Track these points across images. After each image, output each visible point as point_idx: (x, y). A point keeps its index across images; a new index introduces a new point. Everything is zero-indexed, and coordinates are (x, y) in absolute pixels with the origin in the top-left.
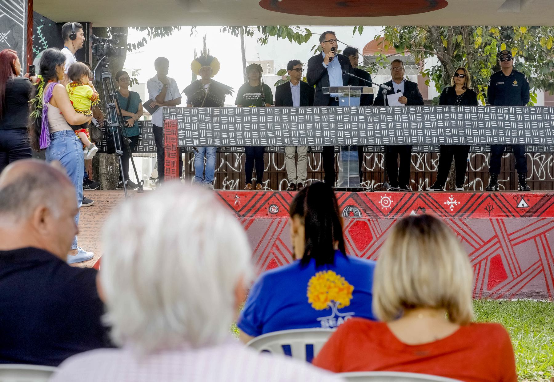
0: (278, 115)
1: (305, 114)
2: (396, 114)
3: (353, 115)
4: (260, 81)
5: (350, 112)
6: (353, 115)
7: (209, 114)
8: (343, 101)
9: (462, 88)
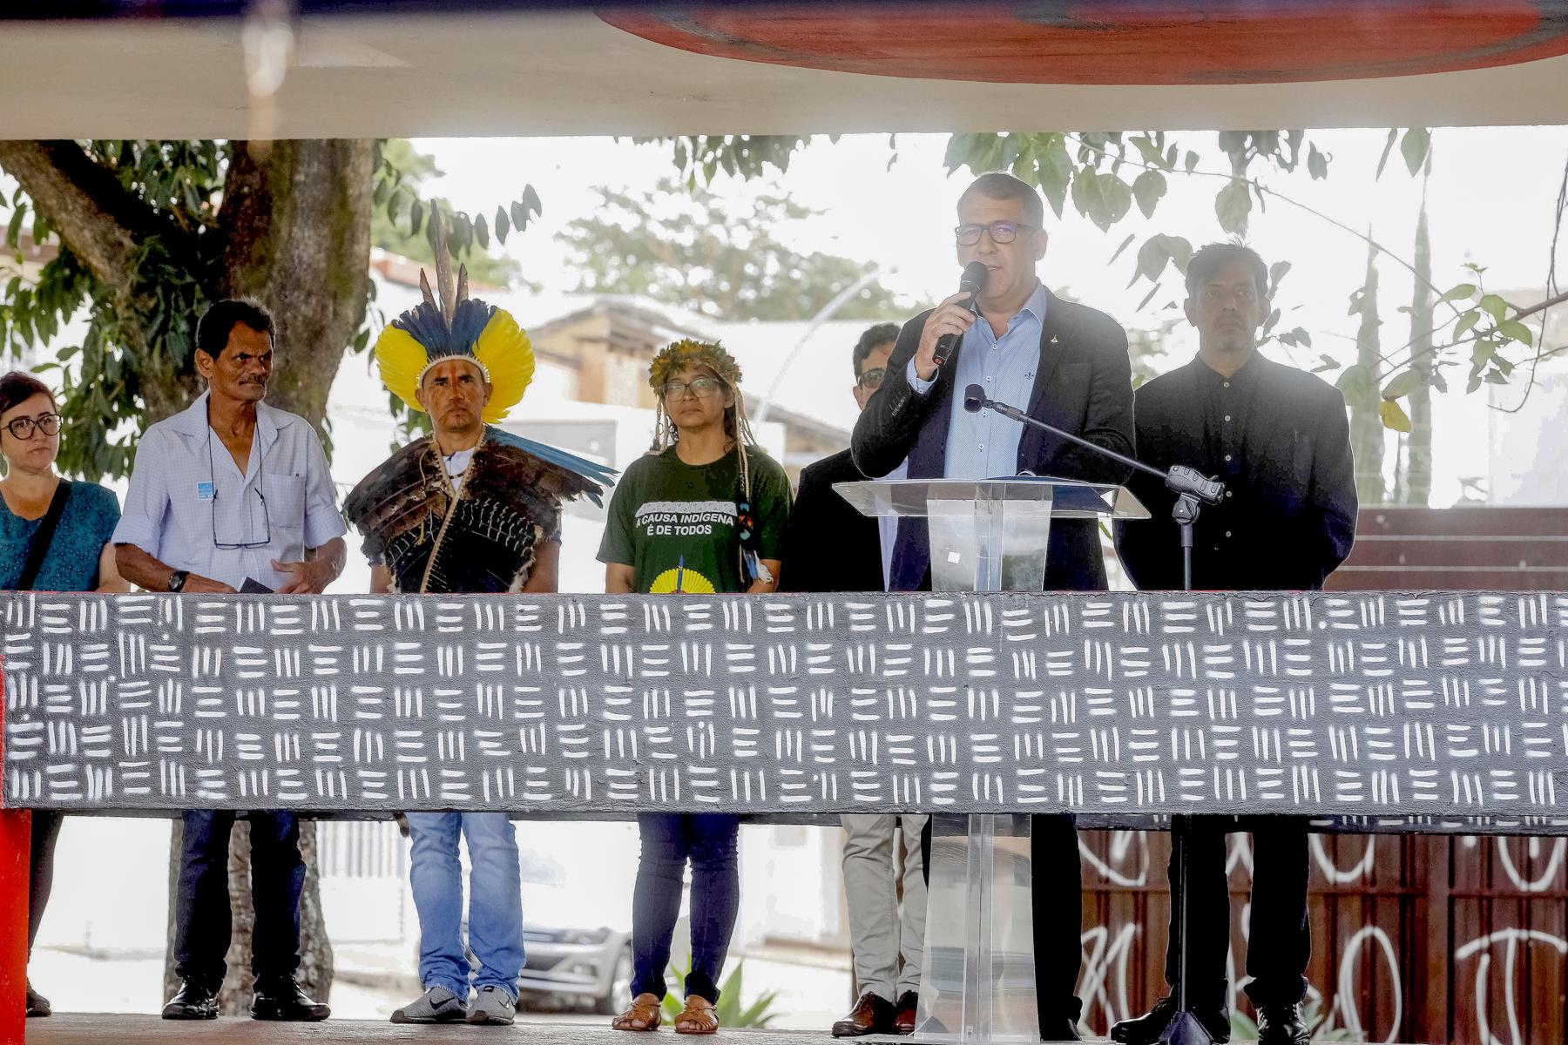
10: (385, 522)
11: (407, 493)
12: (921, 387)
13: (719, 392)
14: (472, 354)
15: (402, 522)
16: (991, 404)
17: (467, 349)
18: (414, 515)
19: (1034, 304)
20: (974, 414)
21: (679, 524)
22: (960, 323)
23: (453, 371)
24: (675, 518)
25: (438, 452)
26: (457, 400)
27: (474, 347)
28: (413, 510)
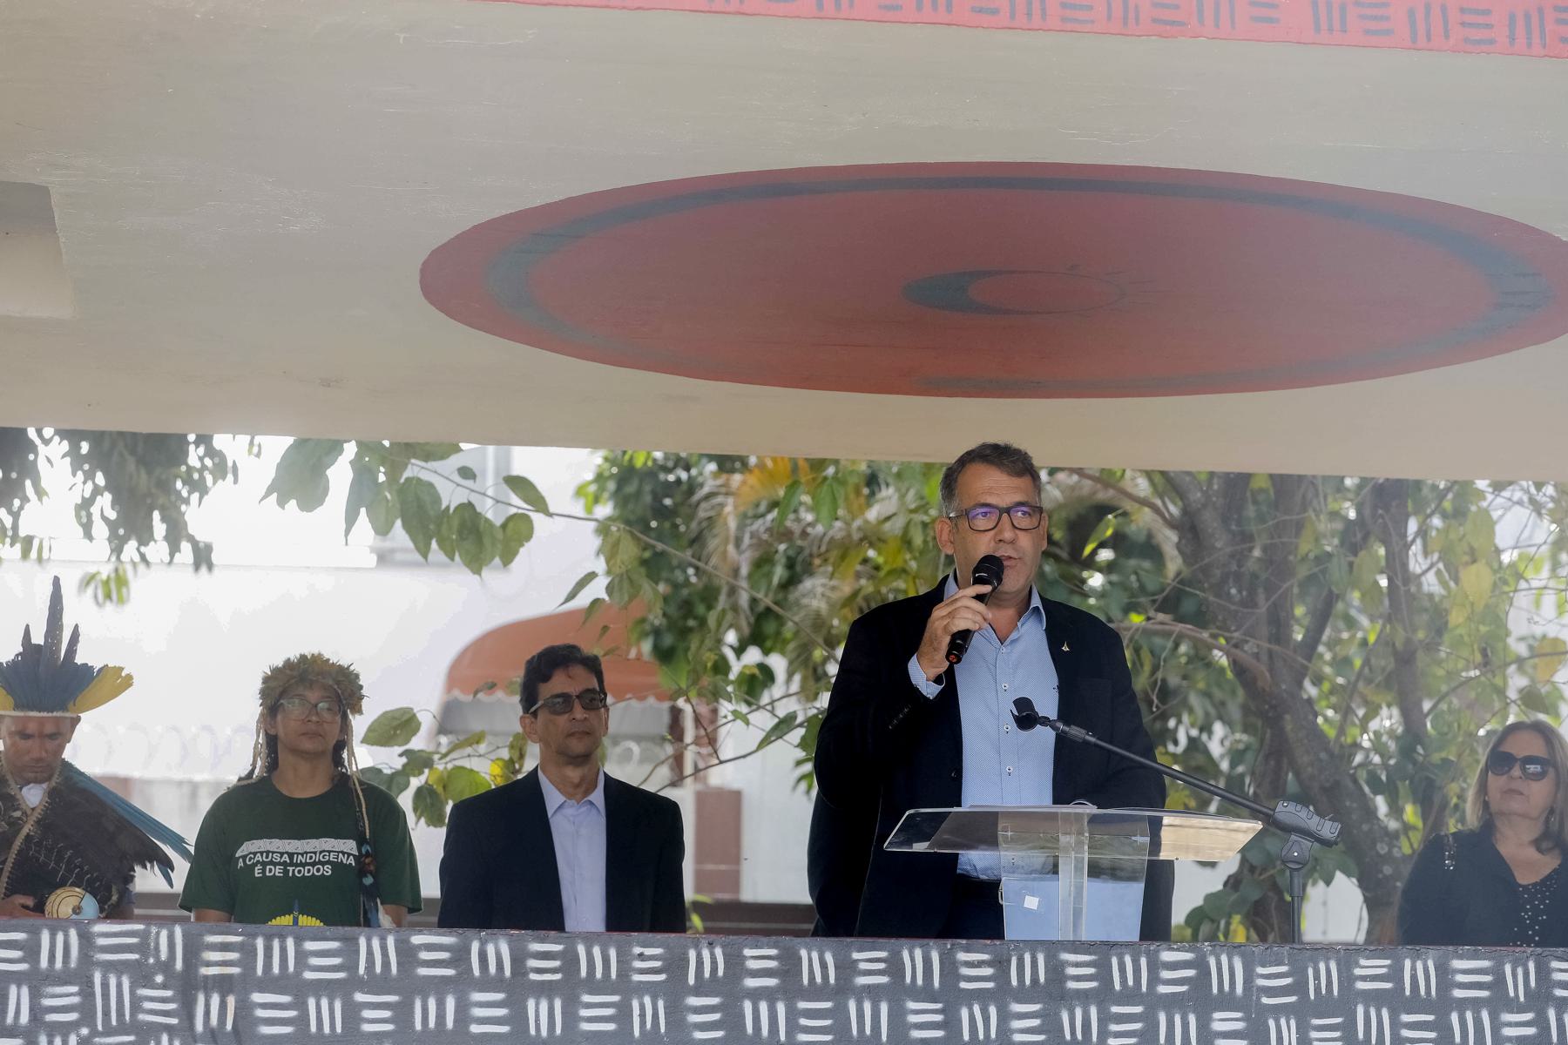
0: (653, 990)
1: (843, 989)
2: (1462, 1005)
3: (1172, 1003)
4: (338, 761)
5: (1154, 980)
6: (1172, 1003)
7: (167, 967)
8: (1031, 902)
9: (1537, 843)
21: (292, 864)
24: (286, 858)
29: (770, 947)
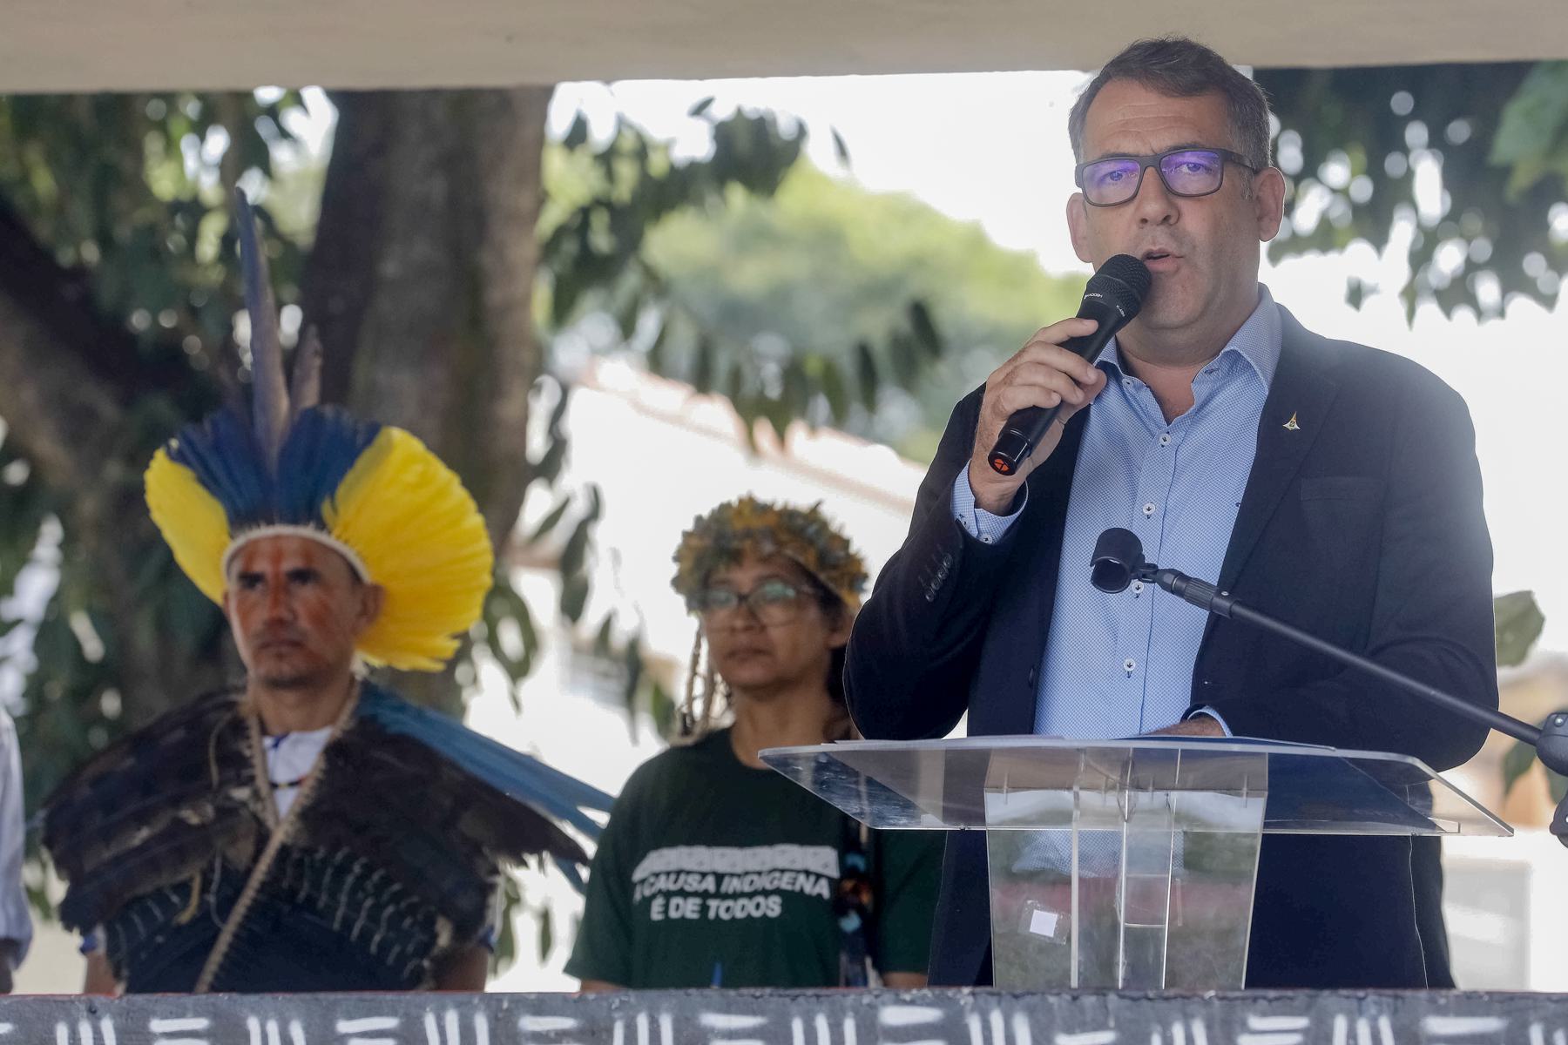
10: (117, 860)
11: (177, 801)
12: (987, 527)
13: (813, 613)
14: (322, 526)
15: (154, 866)
16: (1152, 574)
17: (308, 510)
18: (181, 856)
19: (1252, 342)
20: (1113, 598)
21: (719, 895)
22: (1060, 383)
23: (277, 558)
24: (710, 884)
25: (253, 724)
26: (277, 624)
27: (326, 509)
28: (180, 843)
29: (197, 1015)
